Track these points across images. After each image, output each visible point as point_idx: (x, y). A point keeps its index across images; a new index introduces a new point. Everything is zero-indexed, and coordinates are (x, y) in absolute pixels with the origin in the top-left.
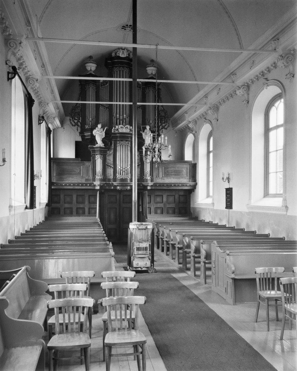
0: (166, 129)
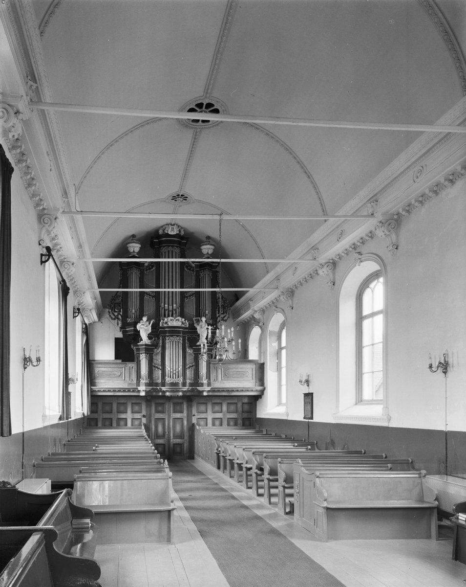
0: (226, 321)
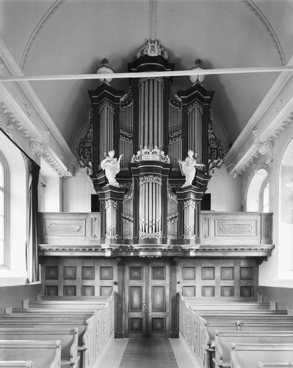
0: (219, 167)
